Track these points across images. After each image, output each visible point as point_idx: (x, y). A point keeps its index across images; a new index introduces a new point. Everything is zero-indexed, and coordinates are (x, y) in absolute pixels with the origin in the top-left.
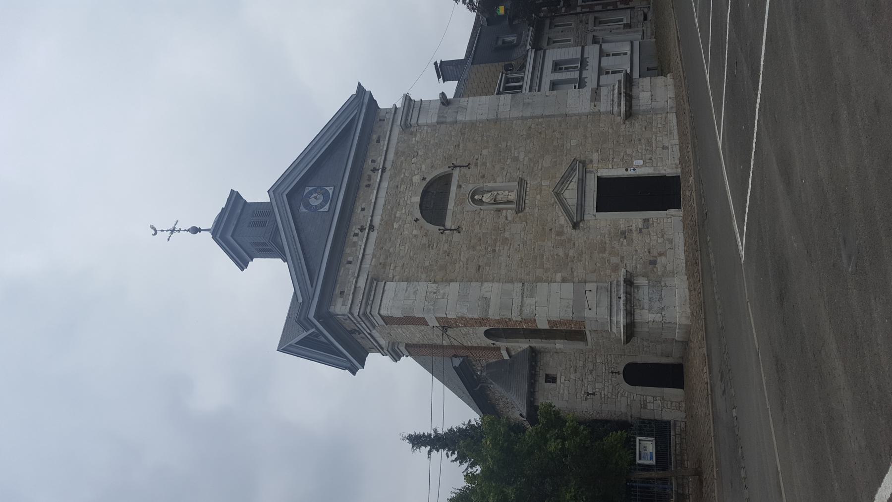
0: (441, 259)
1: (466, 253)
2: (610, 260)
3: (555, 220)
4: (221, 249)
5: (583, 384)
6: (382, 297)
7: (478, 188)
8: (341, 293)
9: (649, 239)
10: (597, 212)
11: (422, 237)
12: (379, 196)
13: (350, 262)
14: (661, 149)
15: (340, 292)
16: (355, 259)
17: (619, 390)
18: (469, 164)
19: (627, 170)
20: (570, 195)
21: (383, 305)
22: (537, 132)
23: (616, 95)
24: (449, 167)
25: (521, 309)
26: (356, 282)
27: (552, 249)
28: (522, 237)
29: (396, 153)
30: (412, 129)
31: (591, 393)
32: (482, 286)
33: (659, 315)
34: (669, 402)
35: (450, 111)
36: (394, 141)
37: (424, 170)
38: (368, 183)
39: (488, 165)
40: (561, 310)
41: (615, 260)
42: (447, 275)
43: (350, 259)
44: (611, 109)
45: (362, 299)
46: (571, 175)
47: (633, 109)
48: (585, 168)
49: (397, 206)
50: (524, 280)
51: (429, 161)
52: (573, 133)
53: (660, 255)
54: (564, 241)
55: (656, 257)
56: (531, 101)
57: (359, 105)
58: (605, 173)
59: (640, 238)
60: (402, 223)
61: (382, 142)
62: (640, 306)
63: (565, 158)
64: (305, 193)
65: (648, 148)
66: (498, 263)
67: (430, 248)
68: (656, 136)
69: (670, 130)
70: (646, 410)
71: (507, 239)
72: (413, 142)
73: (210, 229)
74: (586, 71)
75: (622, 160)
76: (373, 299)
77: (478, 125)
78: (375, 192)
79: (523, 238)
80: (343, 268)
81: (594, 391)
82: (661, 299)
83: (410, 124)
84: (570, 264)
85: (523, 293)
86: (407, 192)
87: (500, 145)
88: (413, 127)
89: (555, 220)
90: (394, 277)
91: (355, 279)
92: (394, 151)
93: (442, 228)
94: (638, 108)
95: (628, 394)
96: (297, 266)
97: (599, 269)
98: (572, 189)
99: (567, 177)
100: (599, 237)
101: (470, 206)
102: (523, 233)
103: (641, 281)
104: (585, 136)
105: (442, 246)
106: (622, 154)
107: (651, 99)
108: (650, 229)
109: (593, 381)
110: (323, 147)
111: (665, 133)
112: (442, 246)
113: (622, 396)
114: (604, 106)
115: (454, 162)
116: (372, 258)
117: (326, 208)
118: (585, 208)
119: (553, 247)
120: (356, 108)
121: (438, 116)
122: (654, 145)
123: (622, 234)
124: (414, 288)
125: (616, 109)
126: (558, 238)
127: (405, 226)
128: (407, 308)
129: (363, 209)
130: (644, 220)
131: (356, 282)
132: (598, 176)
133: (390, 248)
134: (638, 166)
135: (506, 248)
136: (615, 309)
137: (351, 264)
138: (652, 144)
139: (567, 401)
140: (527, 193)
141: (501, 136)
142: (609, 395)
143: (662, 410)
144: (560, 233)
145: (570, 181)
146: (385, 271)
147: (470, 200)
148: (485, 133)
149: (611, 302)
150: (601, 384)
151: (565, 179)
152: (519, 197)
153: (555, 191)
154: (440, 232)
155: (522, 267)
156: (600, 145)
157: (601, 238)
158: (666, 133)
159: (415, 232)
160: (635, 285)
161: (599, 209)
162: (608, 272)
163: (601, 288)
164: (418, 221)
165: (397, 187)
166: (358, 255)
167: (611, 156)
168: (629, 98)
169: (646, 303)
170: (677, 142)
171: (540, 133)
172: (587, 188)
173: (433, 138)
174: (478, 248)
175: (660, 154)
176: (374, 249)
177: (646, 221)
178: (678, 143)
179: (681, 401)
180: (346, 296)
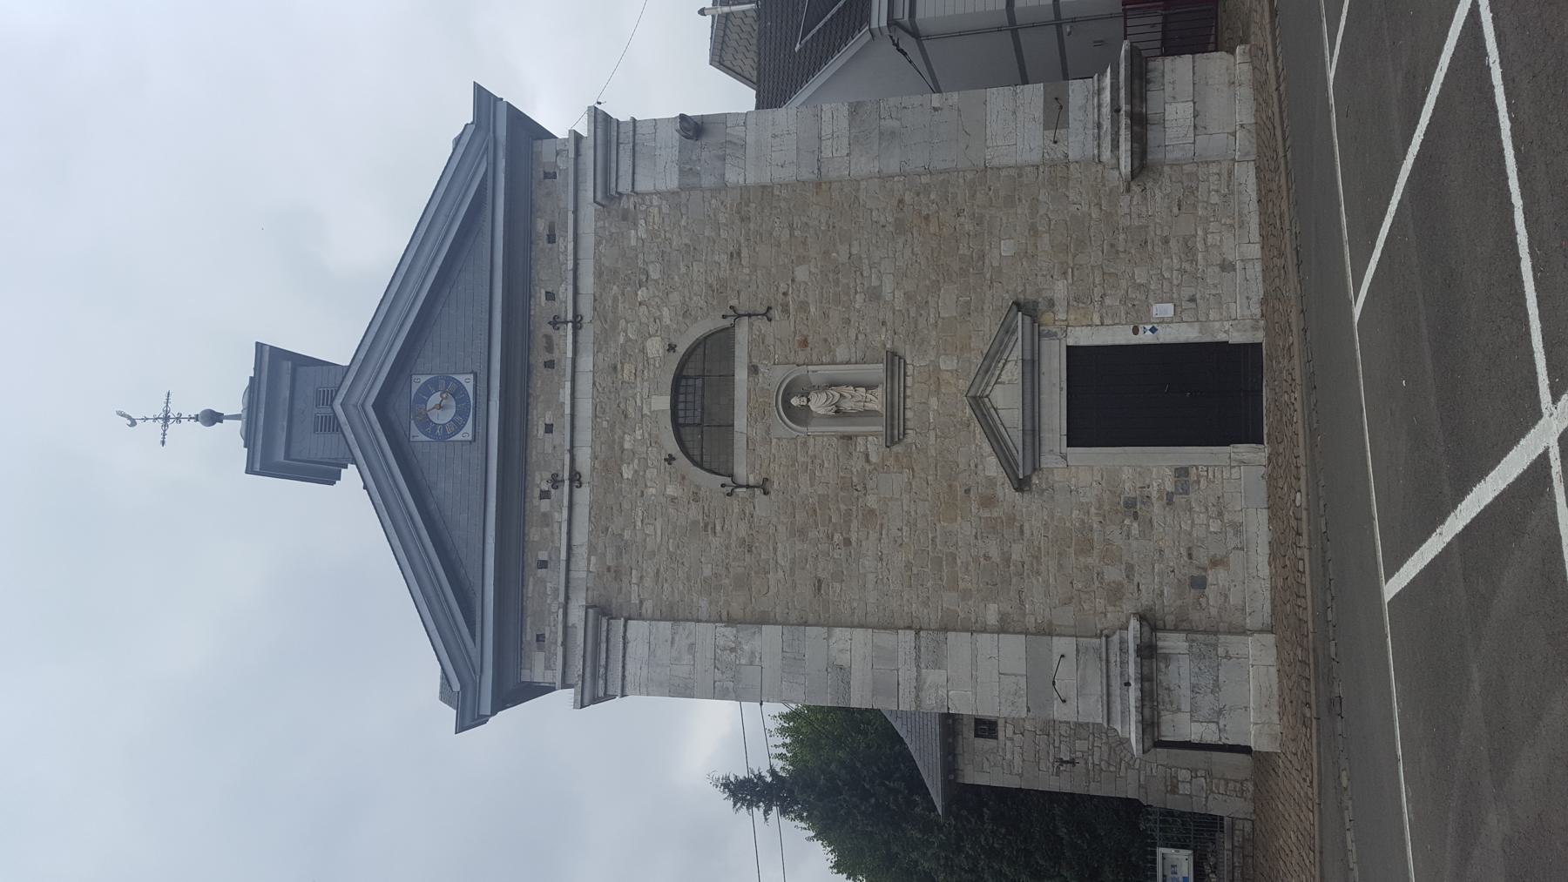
0: (734, 559)
1: (787, 545)
3: (976, 466)
5: (1052, 741)
6: (624, 656)
7: (798, 377)
8: (538, 640)
9: (1189, 522)
10: (1068, 446)
11: (689, 502)
12: (578, 394)
13: (543, 565)
14: (1217, 269)
15: (535, 638)
16: (554, 558)
17: (1122, 755)
18: (769, 308)
19: (1136, 331)
20: (1006, 399)
21: (629, 678)
23: (1106, 110)
24: (724, 317)
26: (565, 614)
27: (972, 541)
28: (905, 508)
29: (599, 274)
30: (624, 203)
31: (1068, 759)
32: (830, 636)
33: (1213, 726)
34: (1222, 782)
35: (705, 154)
36: (588, 241)
37: (668, 322)
38: (548, 357)
39: (813, 310)
40: (1003, 701)
41: (1114, 574)
42: (753, 600)
43: (543, 556)
44: (1096, 152)
45: (584, 669)
46: (1006, 346)
47: (1149, 157)
48: (1037, 325)
49: (623, 419)
50: (917, 617)
51: (675, 297)
52: (1004, 221)
53: (1215, 563)
54: (999, 521)
55: (1205, 569)
56: (896, 124)
57: (487, 148)
58: (1084, 337)
59: (1169, 520)
60: (639, 465)
61: (560, 240)
62: (1171, 703)
64: (414, 391)
65: (1186, 266)
66: (859, 574)
69: (1240, 215)
70: (1177, 796)
71: (872, 512)
72: (633, 243)
73: (240, 415)
75: (1124, 301)
76: (607, 662)
77: (776, 192)
78: (568, 385)
79: (908, 513)
80: (531, 579)
81: (1073, 756)
82: (1216, 687)
83: (617, 192)
84: (1014, 580)
85: (918, 658)
86: (639, 385)
88: (624, 198)
89: (976, 466)
90: (641, 602)
91: (561, 610)
92: (592, 269)
93: (728, 480)
94: (1160, 156)
95: (1140, 764)
96: (432, 594)
98: (1010, 382)
99: (997, 353)
100: (1076, 512)
101: (783, 428)
102: (906, 497)
103: (1173, 643)
104: (1033, 229)
105: (734, 527)
106: (1123, 283)
107: (1195, 126)
108: (1193, 496)
109: (1070, 735)
110: (426, 275)
111: (1229, 221)
112: (734, 527)
113: (1129, 766)
114: (1077, 142)
115: (734, 302)
116: (589, 555)
117: (467, 432)
119: (976, 538)
120: (482, 158)
121: (681, 171)
122: (1200, 256)
124: (687, 637)
125: (1106, 155)
126: (985, 514)
127: (648, 475)
128: (679, 685)
129: (549, 429)
130: (1176, 469)
131: (565, 614)
132: (1068, 347)
133: (623, 530)
134: (1162, 321)
135: (873, 536)
136: (1119, 708)
137: (546, 568)
138: (1195, 255)
139: (1021, 776)
140: (908, 392)
141: (834, 227)
142: (1104, 765)
143: (1207, 798)
144: (988, 501)
145: (1003, 361)
146: (621, 588)
147: (783, 414)
148: (796, 219)
149: (1108, 685)
150: (1087, 742)
151: (993, 359)
152: (890, 405)
153: (972, 393)
154: (724, 489)
155: (911, 586)
156: (1070, 256)
157: (1081, 516)
158: (1232, 222)
159: (670, 491)
160: (1160, 651)
161: (1078, 436)
162: (1100, 603)
163: (1087, 649)
164: (674, 463)
166: (557, 544)
167: (1098, 291)
168: (1140, 123)
169: (1184, 696)
170: (1255, 250)
171: (927, 218)
172: (1044, 382)
174: (812, 534)
176: (590, 533)
177: (1182, 472)
178: (1259, 256)
179: (1246, 780)
180: (550, 647)
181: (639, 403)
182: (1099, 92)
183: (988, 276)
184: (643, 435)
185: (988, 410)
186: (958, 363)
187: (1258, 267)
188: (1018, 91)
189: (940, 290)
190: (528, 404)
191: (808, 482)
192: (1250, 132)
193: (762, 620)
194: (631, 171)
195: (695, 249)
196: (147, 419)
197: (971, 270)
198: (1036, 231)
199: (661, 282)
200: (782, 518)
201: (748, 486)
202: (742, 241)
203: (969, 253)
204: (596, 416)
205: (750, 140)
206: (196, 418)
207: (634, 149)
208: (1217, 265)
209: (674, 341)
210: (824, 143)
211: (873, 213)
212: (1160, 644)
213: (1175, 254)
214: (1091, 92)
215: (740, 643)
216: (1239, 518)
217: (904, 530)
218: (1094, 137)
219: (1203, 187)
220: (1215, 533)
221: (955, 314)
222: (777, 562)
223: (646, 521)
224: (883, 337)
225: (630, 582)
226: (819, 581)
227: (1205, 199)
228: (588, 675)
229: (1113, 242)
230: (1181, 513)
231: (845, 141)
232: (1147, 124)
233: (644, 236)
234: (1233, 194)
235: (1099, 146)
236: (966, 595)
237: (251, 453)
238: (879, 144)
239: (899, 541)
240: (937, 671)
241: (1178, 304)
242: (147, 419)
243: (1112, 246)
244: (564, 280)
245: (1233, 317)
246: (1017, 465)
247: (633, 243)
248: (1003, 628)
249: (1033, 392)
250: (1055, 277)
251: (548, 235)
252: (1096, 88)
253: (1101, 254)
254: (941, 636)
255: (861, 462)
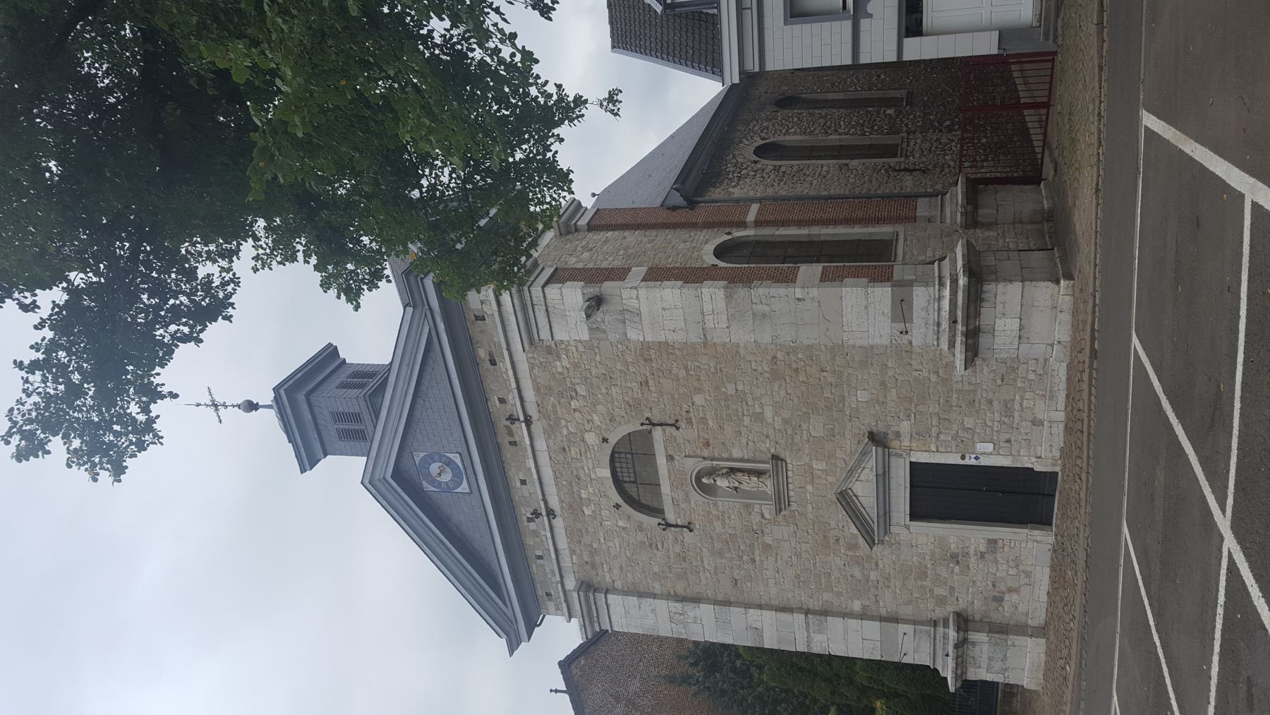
2: (933, 590)
3: (843, 527)
4: (292, 372)
6: (608, 613)
9: (995, 568)
14: (1029, 424)
19: (963, 457)
20: (865, 491)
22: (790, 366)
25: (808, 645)
27: (842, 567)
29: (537, 389)
32: (746, 613)
36: (523, 367)
38: (512, 440)
40: (865, 652)
41: (939, 591)
43: (539, 553)
45: (584, 621)
51: (601, 408)
53: (1010, 590)
55: (1004, 593)
56: (766, 308)
57: (426, 315)
62: (975, 664)
63: (849, 425)
65: (1006, 420)
67: (654, 548)
68: (1022, 398)
69: (1051, 391)
71: (769, 546)
74: (868, 20)
82: (1004, 659)
86: (584, 460)
87: (723, 389)
89: (843, 527)
90: (613, 581)
91: (559, 585)
96: (471, 587)
97: (917, 601)
104: (883, 383)
106: (955, 427)
107: (1020, 337)
108: (999, 556)
117: (464, 487)
118: (891, 513)
119: (845, 565)
123: (953, 558)
130: (988, 540)
132: (911, 462)
135: (771, 559)
140: (790, 480)
157: (919, 560)
159: (621, 523)
160: (969, 640)
161: (915, 515)
162: (931, 606)
165: (564, 449)
167: (934, 430)
170: (1061, 416)
171: (797, 370)
172: (893, 483)
173: (593, 364)
175: (1027, 434)
176: (569, 543)
177: (992, 542)
181: (587, 471)
182: (940, 298)
183: (848, 413)
184: (594, 490)
185: (850, 498)
186: (827, 466)
187: (1061, 426)
188: (869, 292)
189: (810, 419)
190: (504, 467)
191: (721, 526)
192: (1065, 347)
193: (697, 600)
194: (548, 327)
195: (611, 377)
196: (200, 405)
197: (834, 408)
198: (886, 386)
199: (588, 397)
200: (704, 544)
201: (677, 526)
202: (648, 375)
203: (832, 397)
204: (557, 477)
205: (644, 309)
206: (239, 406)
207: (547, 310)
208: (1029, 421)
209: (606, 436)
210: (707, 317)
211: (753, 364)
212: (969, 637)
213: (998, 411)
214: (933, 297)
215: (686, 612)
216: (1029, 569)
217: (793, 558)
218: (934, 332)
219: (1022, 368)
220: (1013, 575)
221: (823, 435)
222: (704, 568)
223: (607, 539)
224: (768, 445)
225: (603, 571)
226: (736, 580)
227: (1024, 376)
228: (587, 623)
229: (948, 399)
230: (990, 564)
231: (724, 317)
232: (979, 332)
233: (568, 366)
234: (1047, 374)
235: (938, 339)
236: (839, 594)
237: (295, 445)
238: (754, 322)
239: (790, 563)
240: (821, 635)
241: (996, 443)
242: (200, 405)
243: (947, 401)
244: (510, 391)
245: (1039, 455)
246: (873, 532)
247: (560, 370)
248: (863, 616)
249: (885, 491)
250: (901, 418)
251: (490, 360)
252: (937, 296)
253: (937, 406)
254: (823, 618)
255: (758, 518)
